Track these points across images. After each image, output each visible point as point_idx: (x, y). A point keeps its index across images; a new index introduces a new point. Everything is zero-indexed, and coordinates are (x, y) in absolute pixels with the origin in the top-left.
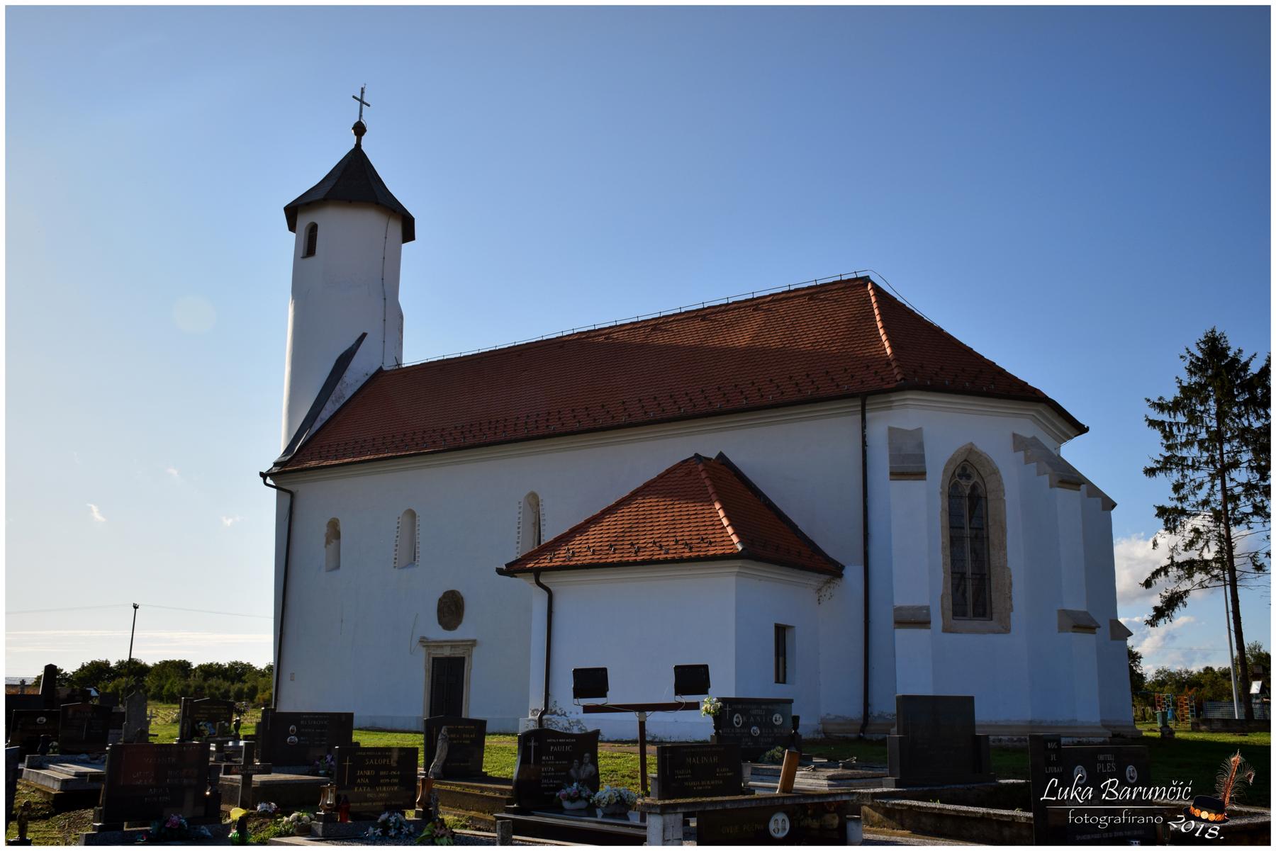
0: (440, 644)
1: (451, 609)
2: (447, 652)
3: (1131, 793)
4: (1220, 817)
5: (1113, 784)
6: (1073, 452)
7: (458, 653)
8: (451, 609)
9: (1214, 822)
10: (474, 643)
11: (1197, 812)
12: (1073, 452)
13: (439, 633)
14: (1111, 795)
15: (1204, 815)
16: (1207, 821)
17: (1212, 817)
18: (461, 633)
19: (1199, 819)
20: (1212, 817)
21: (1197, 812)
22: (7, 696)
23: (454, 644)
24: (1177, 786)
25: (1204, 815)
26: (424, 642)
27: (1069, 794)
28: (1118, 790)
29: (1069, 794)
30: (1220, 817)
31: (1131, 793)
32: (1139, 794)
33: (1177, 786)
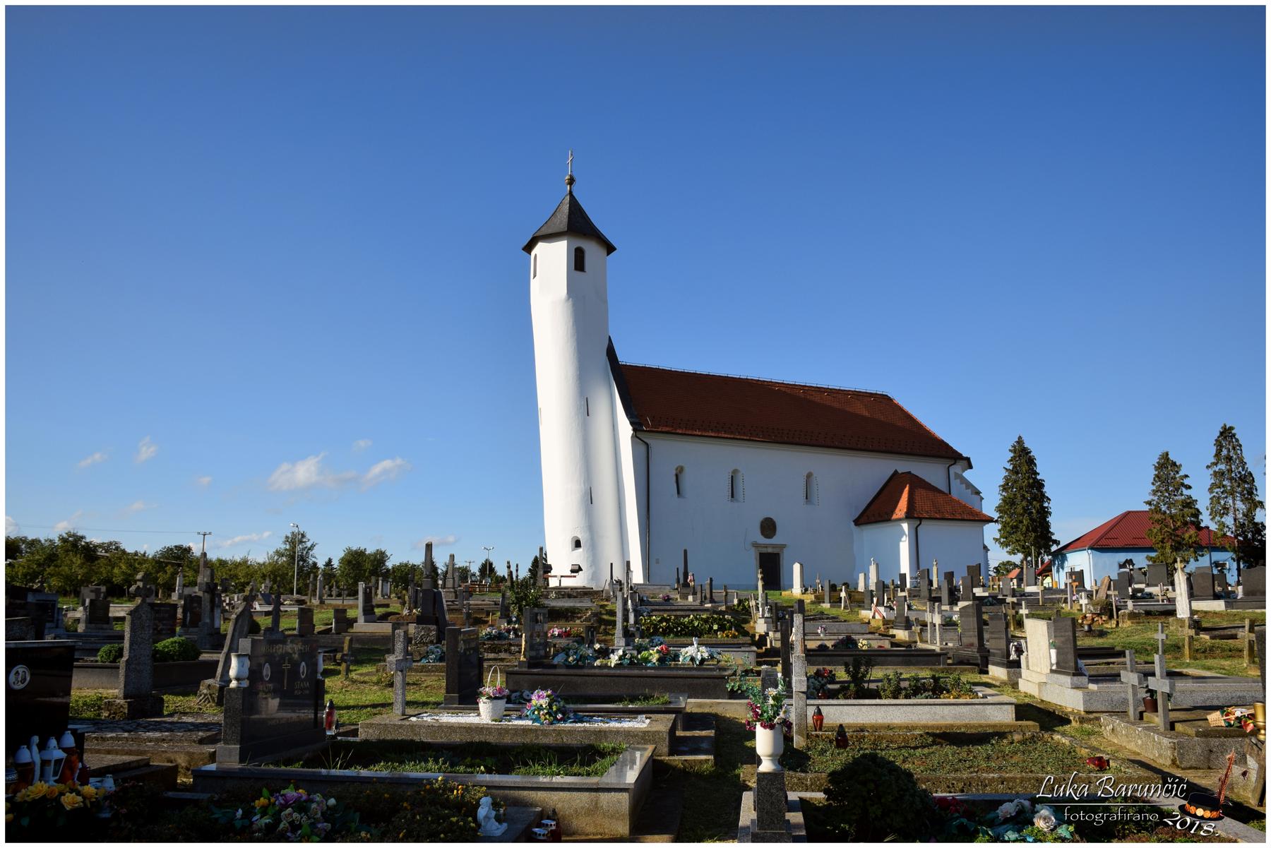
0: (766, 546)
1: (768, 527)
2: (770, 550)
3: (1127, 789)
4: (1215, 814)
6: (968, 474)
7: (776, 551)
8: (768, 527)
9: (1210, 819)
10: (783, 546)
11: (1192, 809)
12: (968, 474)
13: (762, 540)
15: (1200, 812)
16: (1202, 818)
17: (1208, 814)
18: (775, 540)
19: (1195, 816)
20: (1208, 814)
21: (1192, 809)
22: (7, 650)
23: (774, 546)
24: (1172, 783)
25: (1200, 812)
26: (755, 545)
27: (1064, 791)
28: (1114, 786)
29: (1064, 791)
31: (1127, 789)
32: (1135, 791)
33: (1172, 783)
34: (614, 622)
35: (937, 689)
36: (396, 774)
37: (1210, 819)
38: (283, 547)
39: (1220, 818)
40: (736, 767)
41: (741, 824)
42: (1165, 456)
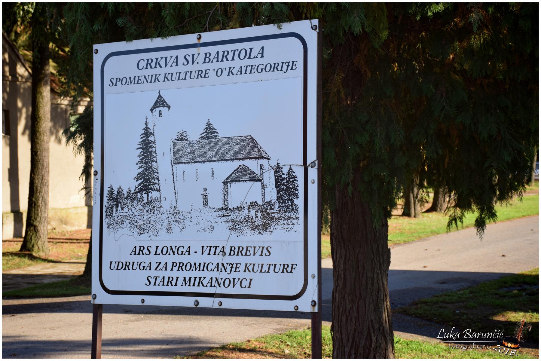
3: (477, 335)
4: (516, 346)
5: (469, 331)
9: (514, 348)
11: (506, 344)
14: (467, 336)
15: (509, 345)
16: (510, 348)
17: (513, 346)
19: (507, 347)
21: (506, 344)
25: (509, 345)
27: (449, 336)
28: (471, 334)
29: (449, 336)
30: (516, 346)
31: (477, 335)
32: (480, 336)
33: (497, 332)
34: (297, 218)
35: (386, 296)
36: (48, 116)
37: (514, 348)
38: (143, 132)
39: (518, 348)
40: (477, 204)
41: (391, 268)
42: (209, 125)
